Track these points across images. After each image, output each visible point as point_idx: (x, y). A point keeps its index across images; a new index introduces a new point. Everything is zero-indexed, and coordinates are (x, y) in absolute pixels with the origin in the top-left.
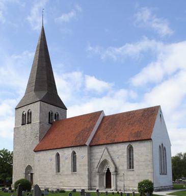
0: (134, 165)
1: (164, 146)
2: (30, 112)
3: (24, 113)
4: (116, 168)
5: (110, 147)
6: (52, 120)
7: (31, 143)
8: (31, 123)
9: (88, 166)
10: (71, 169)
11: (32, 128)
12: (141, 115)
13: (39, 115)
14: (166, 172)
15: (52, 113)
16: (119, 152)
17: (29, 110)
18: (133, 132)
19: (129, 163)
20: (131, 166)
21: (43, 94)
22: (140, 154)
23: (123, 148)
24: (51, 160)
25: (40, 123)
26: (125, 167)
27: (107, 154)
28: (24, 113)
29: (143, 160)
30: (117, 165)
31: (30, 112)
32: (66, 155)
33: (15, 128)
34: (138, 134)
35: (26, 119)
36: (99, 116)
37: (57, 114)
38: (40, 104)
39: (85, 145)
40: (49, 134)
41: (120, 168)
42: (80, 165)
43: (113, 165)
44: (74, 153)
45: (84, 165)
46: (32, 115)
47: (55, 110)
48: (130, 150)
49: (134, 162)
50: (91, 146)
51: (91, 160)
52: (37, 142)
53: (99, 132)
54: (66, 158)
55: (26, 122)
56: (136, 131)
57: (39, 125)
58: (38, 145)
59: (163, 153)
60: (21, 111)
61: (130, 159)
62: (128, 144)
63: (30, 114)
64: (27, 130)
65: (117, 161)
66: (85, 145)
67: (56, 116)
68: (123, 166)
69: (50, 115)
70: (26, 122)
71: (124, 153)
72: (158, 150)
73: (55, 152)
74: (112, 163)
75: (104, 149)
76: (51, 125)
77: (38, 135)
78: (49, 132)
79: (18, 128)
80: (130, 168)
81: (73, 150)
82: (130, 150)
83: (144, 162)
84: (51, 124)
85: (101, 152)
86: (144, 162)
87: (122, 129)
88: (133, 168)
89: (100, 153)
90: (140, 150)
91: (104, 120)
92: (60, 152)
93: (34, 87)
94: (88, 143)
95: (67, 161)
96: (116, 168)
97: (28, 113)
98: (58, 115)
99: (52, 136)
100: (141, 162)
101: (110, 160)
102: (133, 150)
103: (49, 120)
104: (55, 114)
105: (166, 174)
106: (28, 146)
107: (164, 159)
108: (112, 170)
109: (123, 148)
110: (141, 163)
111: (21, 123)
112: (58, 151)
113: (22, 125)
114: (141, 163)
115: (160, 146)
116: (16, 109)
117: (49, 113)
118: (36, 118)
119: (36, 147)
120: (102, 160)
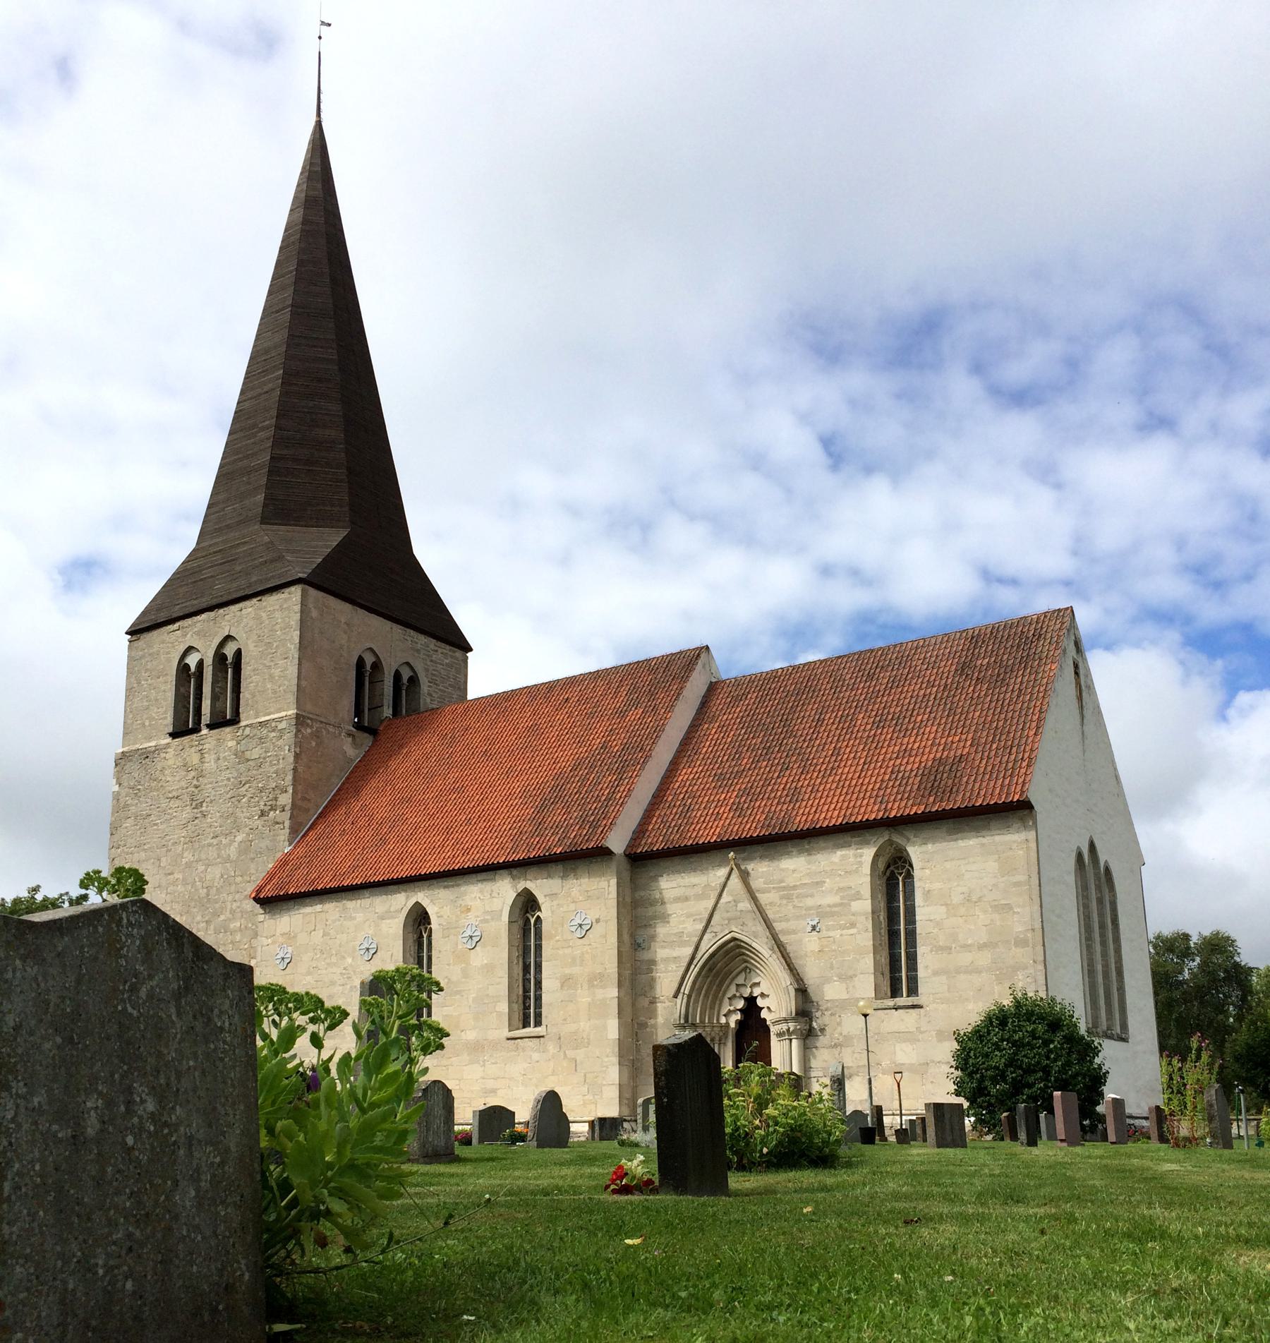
0: (921, 973)
1: (1103, 858)
2: (229, 651)
3: (192, 661)
4: (802, 992)
5: (762, 870)
6: (375, 708)
7: (233, 851)
8: (235, 721)
9: (620, 985)
10: (504, 1007)
11: (240, 756)
12: (949, 667)
13: (293, 671)
14: (1124, 1026)
15: (377, 666)
16: (822, 896)
17: (229, 638)
18: (911, 765)
19: (885, 960)
20: (898, 974)
21: (324, 541)
22: (956, 899)
23: (853, 866)
24: (288, 962)
25: (300, 720)
26: (865, 984)
27: (746, 905)
28: (192, 661)
29: (983, 937)
30: (811, 974)
31: (229, 651)
32: (472, 918)
33: (122, 760)
34: (938, 775)
35: (204, 700)
36: (684, 679)
37: (369, 660)
38: (303, 604)
39: (595, 855)
40: (357, 791)
41: (829, 992)
42: (566, 982)
43: (785, 979)
44: (527, 904)
45: (595, 980)
46: (246, 670)
47: (394, 645)
48: (894, 878)
49: (922, 951)
50: (643, 861)
51: (637, 946)
52: (279, 843)
53: (684, 774)
54: (476, 941)
55: (206, 718)
56: (928, 759)
57: (289, 737)
58: (283, 862)
59: (1100, 901)
60: (169, 644)
61: (893, 935)
62: (883, 837)
63: (229, 666)
64: (210, 765)
65: (806, 947)
66: (603, 853)
67: (406, 687)
68: (846, 978)
69: (366, 674)
70: (206, 718)
71: (857, 896)
72: (1071, 879)
73: (401, 902)
74: (773, 963)
75: (723, 872)
76: (367, 740)
77: (286, 799)
78: (355, 780)
79: (146, 755)
80: (895, 992)
81: (522, 885)
82: (894, 878)
83: (982, 947)
84: (372, 731)
85: (700, 897)
86: (982, 947)
87: (837, 752)
88: (913, 991)
89: (691, 905)
90: (953, 873)
91: (717, 704)
92: (435, 901)
93: (260, 498)
94: (617, 842)
95: (479, 958)
96: (802, 992)
97: (220, 658)
98: (414, 680)
99: (376, 799)
100: (966, 947)
101: (762, 945)
102: (909, 876)
103: (358, 711)
104: (397, 676)
105: (1125, 1040)
106: (215, 872)
107: (1104, 943)
108: (776, 1006)
109: (853, 866)
110: (965, 959)
111: (167, 720)
112: (422, 896)
113: (174, 735)
114: (965, 959)
115: (1080, 856)
116: (136, 632)
117: (360, 663)
118: (272, 693)
119: (271, 876)
120: (709, 945)
